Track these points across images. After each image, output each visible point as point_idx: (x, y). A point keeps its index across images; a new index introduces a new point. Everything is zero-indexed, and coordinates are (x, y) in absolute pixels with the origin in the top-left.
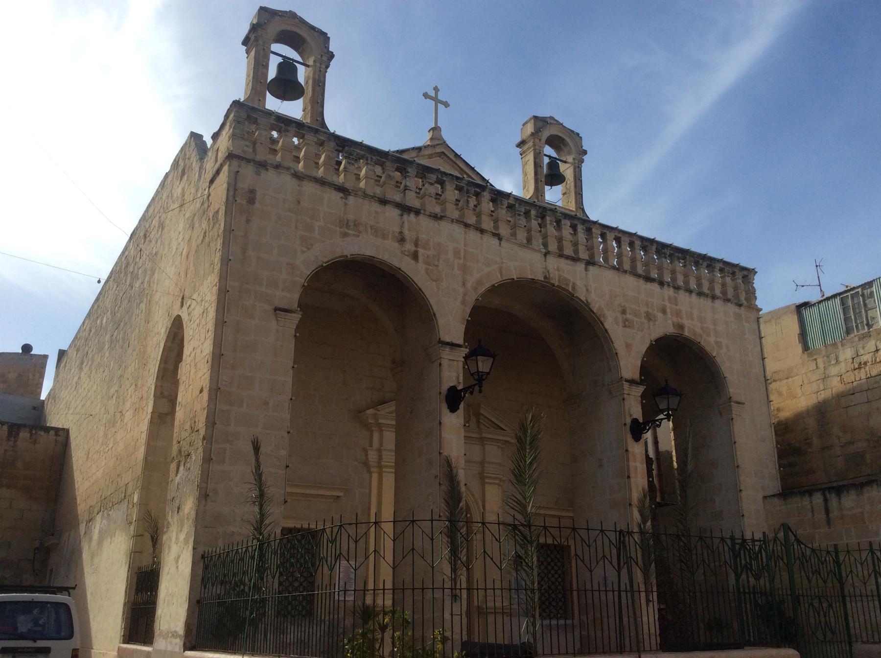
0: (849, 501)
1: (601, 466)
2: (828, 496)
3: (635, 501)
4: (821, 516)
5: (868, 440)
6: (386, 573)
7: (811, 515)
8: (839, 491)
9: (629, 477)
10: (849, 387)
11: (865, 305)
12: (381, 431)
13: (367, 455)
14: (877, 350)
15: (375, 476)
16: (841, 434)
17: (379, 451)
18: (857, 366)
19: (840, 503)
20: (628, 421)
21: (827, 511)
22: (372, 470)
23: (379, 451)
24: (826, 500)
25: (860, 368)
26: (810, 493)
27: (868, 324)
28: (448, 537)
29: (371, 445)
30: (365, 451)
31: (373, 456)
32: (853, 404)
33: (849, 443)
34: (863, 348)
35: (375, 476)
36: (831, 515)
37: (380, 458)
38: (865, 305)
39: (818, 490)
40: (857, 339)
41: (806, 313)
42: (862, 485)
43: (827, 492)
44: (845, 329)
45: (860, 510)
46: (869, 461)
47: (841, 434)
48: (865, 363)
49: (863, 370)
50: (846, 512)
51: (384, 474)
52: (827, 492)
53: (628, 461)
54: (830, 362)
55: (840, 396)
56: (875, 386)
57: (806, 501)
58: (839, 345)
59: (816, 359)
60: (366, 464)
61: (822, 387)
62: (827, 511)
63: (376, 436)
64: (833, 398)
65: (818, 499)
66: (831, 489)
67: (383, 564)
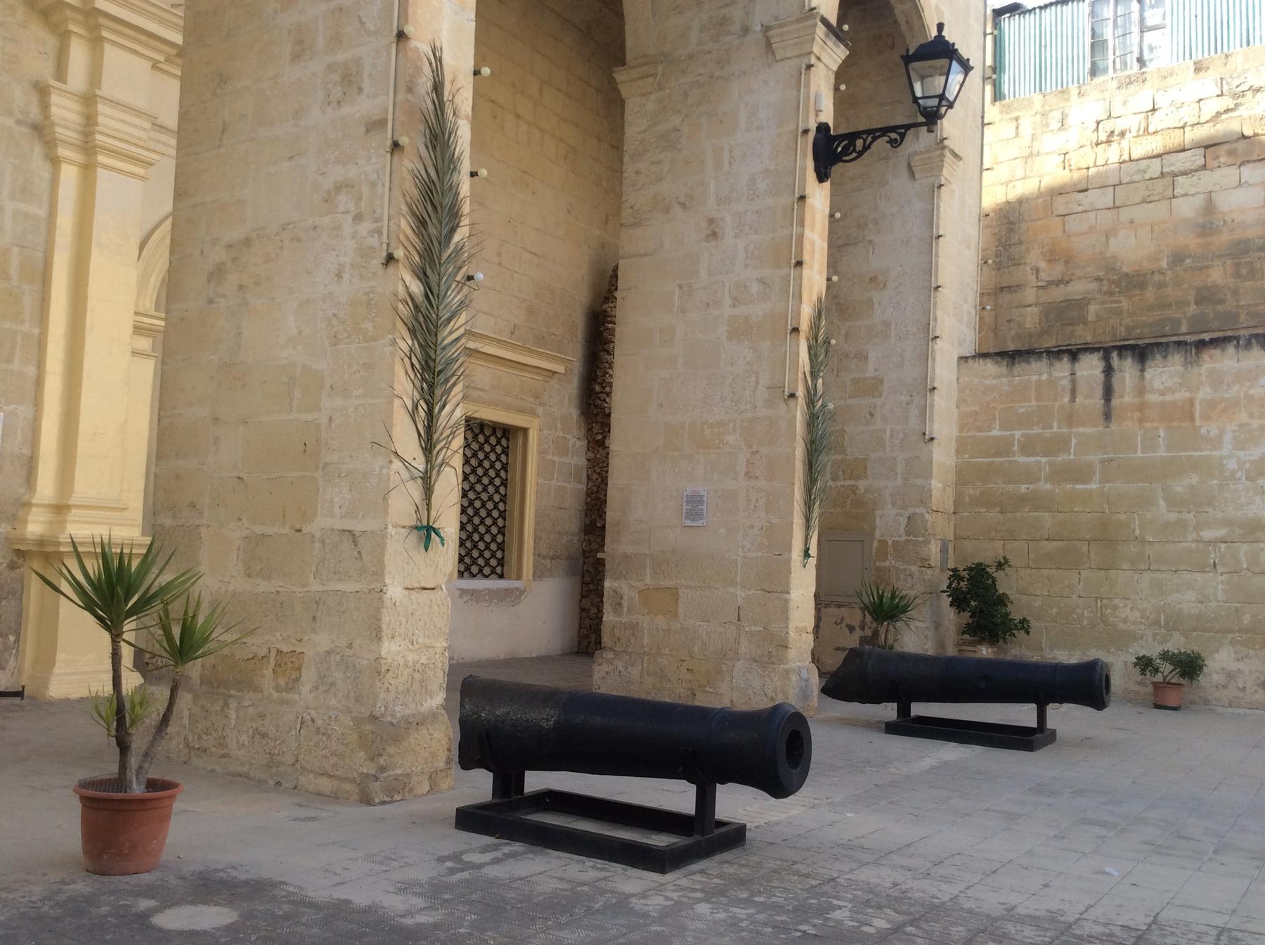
0: (1165, 376)
1: (714, 235)
2: (1115, 361)
3: (804, 326)
4: (1091, 400)
5: (1098, 279)
6: (1127, 376)
7: (1067, 399)
8: (1142, 353)
9: (799, 264)
10: (1076, 175)
11: (1142, 20)
12: (96, 43)
13: (45, 106)
14: (1154, 110)
15: (69, 175)
16: (1042, 265)
17: (89, 100)
18: (1103, 137)
19: (1142, 377)
20: (813, 126)
21: (1108, 392)
22: (62, 152)
23: (89, 100)
24: (1108, 371)
25: (1109, 142)
26: (1074, 355)
27: (1141, 61)
28: (413, 332)
29: (61, 72)
30: (42, 91)
31: (64, 110)
32: (1080, 209)
33: (1058, 283)
34: (1125, 103)
35: (69, 175)
36: (1115, 402)
37: (90, 120)
38: (1142, 20)
39: (1089, 349)
40: (1115, 84)
41: (1010, 25)
42: (1201, 345)
43: (1114, 354)
44: (1088, 66)
45: (1187, 395)
46: (1091, 317)
47: (1042, 265)
48: (1122, 134)
49: (1114, 145)
50: (1152, 398)
51: (100, 172)
52: (1114, 354)
53: (801, 223)
54: (1047, 125)
55: (1059, 192)
56: (1136, 178)
57: (1062, 369)
58: (1074, 91)
59: (1017, 119)
60: (42, 130)
61: (1019, 173)
62: (1108, 392)
63: (78, 54)
64: (1040, 195)
65: (1091, 367)
66: (1122, 350)
67: (483, 350)
